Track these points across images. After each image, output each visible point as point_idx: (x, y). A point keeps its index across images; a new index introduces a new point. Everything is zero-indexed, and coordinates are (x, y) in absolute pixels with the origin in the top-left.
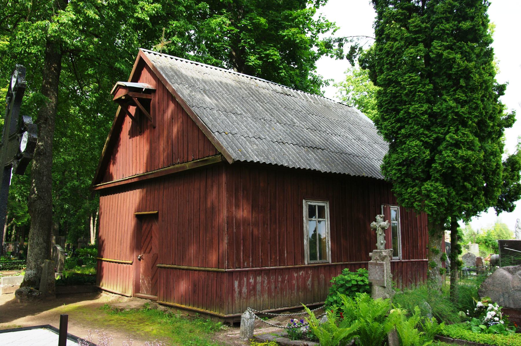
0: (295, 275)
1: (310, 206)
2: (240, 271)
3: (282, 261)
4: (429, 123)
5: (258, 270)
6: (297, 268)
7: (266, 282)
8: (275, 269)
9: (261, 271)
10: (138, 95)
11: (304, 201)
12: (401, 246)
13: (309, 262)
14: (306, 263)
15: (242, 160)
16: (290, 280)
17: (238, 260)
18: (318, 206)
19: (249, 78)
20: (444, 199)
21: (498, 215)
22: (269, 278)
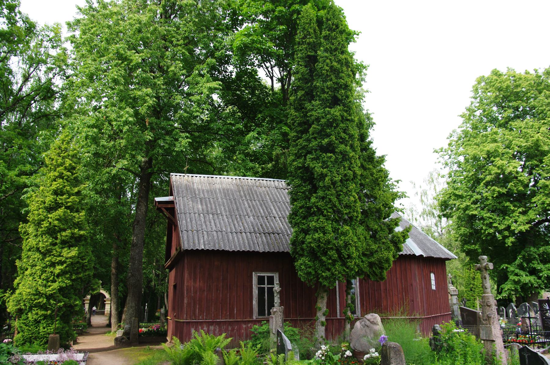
0: (244, 326)
1: (259, 276)
2: (195, 322)
3: (231, 315)
4: (277, 86)
5: (211, 322)
6: (246, 321)
7: (218, 330)
8: (226, 321)
9: (213, 322)
10: (165, 206)
11: (253, 273)
12: (359, 306)
13: (258, 317)
14: (254, 318)
15: (276, 251)
16: (240, 329)
17: (194, 314)
18: (267, 276)
19: (218, 178)
20: (310, 270)
21: (508, 67)
22: (220, 327)
